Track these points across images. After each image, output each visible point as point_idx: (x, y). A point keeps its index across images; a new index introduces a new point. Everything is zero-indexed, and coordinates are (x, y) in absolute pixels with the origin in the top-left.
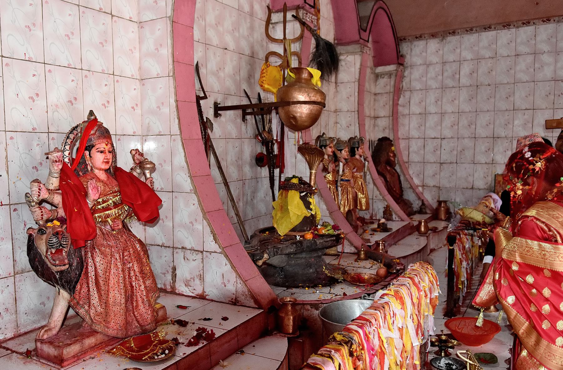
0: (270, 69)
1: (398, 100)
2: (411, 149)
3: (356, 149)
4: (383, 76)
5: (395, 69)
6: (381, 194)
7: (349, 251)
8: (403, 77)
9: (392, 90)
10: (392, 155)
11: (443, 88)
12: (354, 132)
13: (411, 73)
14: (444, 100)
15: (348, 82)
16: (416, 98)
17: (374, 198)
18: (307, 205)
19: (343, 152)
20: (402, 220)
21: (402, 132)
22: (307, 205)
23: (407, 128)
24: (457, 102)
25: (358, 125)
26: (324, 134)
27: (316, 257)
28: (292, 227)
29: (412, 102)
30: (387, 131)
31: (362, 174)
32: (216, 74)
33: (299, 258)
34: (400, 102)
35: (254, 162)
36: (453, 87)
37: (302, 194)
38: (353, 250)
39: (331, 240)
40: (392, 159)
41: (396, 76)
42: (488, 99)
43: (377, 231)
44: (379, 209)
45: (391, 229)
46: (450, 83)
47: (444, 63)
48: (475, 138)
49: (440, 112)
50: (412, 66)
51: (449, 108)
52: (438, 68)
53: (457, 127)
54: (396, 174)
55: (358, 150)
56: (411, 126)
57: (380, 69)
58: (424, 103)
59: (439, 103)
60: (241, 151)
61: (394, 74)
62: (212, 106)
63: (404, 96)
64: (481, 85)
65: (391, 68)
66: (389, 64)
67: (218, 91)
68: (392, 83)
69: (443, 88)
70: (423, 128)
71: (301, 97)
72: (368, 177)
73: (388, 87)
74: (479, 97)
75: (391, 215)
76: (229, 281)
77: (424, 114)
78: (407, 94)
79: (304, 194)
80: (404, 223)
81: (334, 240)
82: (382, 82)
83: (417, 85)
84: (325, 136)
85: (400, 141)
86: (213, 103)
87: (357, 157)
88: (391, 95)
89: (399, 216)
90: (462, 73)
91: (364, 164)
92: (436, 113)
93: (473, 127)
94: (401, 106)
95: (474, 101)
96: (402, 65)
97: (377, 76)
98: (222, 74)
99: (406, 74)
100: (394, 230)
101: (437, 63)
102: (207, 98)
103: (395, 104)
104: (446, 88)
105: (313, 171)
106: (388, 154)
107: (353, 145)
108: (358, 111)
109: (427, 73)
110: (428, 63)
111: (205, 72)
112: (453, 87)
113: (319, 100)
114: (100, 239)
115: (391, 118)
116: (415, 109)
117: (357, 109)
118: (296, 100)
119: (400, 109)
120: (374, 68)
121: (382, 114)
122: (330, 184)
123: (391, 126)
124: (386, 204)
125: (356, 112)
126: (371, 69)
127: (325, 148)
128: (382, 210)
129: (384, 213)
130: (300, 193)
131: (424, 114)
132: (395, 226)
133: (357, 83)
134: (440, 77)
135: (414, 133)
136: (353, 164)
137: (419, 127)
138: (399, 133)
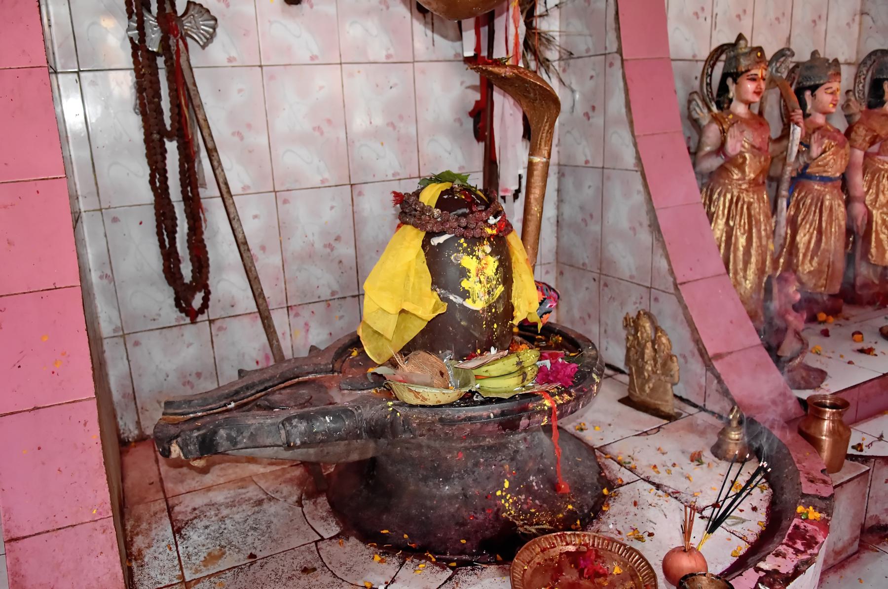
19: (820, 93)
26: (740, 37)
84: (742, 42)
127: (735, 81)
130: (430, 235)
136: (870, 130)
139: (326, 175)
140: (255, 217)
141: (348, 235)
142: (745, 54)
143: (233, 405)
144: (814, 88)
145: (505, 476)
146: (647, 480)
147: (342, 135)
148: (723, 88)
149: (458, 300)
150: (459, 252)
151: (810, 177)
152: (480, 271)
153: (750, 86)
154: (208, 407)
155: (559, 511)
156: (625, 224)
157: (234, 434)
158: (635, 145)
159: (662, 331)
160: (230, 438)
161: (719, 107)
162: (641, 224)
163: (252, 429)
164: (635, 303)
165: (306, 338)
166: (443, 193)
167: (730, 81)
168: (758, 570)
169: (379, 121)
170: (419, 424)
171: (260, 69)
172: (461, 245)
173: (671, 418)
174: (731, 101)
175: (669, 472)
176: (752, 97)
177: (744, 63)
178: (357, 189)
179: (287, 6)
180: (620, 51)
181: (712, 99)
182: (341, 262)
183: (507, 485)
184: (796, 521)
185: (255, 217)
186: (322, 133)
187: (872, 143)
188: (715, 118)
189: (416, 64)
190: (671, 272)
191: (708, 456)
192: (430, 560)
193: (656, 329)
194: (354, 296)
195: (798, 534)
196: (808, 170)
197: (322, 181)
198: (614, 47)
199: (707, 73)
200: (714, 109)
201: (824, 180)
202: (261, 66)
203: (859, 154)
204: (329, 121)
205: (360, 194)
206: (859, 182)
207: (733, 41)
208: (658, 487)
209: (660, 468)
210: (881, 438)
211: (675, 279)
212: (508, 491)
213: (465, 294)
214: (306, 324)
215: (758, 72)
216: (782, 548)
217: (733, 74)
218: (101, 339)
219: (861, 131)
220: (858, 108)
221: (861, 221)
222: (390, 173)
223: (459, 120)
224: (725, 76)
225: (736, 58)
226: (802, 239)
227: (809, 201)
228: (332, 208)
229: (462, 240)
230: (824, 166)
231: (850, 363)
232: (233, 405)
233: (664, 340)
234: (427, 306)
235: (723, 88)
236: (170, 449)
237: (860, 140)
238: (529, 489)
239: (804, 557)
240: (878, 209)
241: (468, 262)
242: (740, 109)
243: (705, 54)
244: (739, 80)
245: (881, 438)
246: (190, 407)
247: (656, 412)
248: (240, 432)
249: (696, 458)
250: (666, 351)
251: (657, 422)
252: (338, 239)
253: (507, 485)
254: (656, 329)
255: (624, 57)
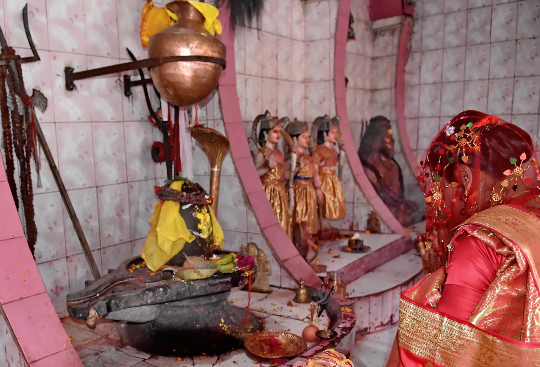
0: (152, 12)
1: (405, 65)
2: (421, 133)
3: (325, 134)
4: (383, 33)
5: (399, 21)
6: (364, 196)
7: (287, 286)
8: (411, 33)
9: (395, 51)
10: (388, 140)
11: (467, 45)
12: (329, 109)
13: (422, 27)
14: (468, 63)
15: (321, 39)
16: (428, 61)
17: (356, 201)
18: (193, 225)
19: (300, 137)
20: (393, 232)
21: (409, 109)
22: (193, 225)
23: (416, 103)
24: (486, 64)
25: (333, 100)
26: (267, 112)
27: (208, 304)
28: (167, 259)
29: (423, 67)
30: (388, 108)
31: (336, 168)
32: (69, 23)
33: (178, 307)
34: (407, 68)
35: (149, 154)
36: (482, 43)
37: (185, 207)
38: (293, 284)
39: (222, 283)
40: (389, 146)
41: (401, 31)
42: (533, 58)
43: (347, 251)
44: (361, 217)
45: (369, 248)
46: (478, 37)
47: (469, 10)
48: (512, 114)
49: (462, 79)
50: (424, 18)
51: (475, 74)
52: (461, 17)
53: (486, 100)
54: (396, 167)
55: (327, 135)
56: (422, 99)
57: (380, 24)
58: (439, 69)
59: (462, 66)
60: (125, 140)
61: (398, 30)
62: (62, 73)
63: (413, 60)
64: (522, 38)
65: (393, 21)
66: (391, 16)
67: (73, 50)
68: (396, 41)
69: (467, 45)
70: (437, 103)
71: (185, 51)
72: (346, 172)
73: (390, 48)
74: (519, 57)
75: (378, 225)
76: (12, 359)
77: (440, 84)
78: (417, 57)
79: (187, 206)
80: (397, 237)
81: (228, 283)
82: (382, 40)
83: (431, 43)
84: (268, 115)
85: (407, 121)
86: (62, 68)
87: (327, 144)
88: (394, 59)
89: (388, 227)
90: (494, 23)
91: (339, 156)
92: (456, 81)
93: (509, 99)
94: (408, 73)
95: (512, 62)
96: (410, 16)
97: (376, 34)
98: (79, 24)
99: (416, 28)
100: (374, 248)
101: (459, 10)
102: (39, 59)
103: (400, 71)
104: (472, 45)
105: (216, 169)
106: (383, 139)
107: (322, 127)
108: (334, 80)
109: (445, 25)
110: (446, 11)
111: (116, 32)
112: (482, 43)
113: (216, 55)
114: (428, 170)
115: (393, 90)
116: (428, 77)
117: (332, 77)
118: (167, 55)
119: (407, 77)
120: (370, 22)
121: (382, 84)
122: (275, 185)
123: (393, 102)
124: (372, 209)
125: (332, 82)
126: (366, 23)
127: (267, 133)
128: (365, 219)
129: (369, 222)
130: (182, 204)
131: (440, 84)
132: (374, 243)
133: (333, 41)
134: (464, 31)
135: (426, 110)
136: (320, 155)
137: (433, 101)
138: (406, 111)
139: (85, 182)
140: (52, 205)
141: (95, 215)
142: (271, 120)
143: (98, 295)
144: (297, 136)
145: (221, 317)
146: (274, 315)
147: (92, 160)
148: (262, 136)
149: (197, 234)
150: (195, 211)
151: (300, 178)
152: (205, 220)
153: (274, 135)
154: (89, 296)
155: (248, 329)
156: (230, 203)
157: (117, 302)
158: (234, 163)
159: (261, 251)
160: (116, 304)
161: (261, 145)
162: (240, 202)
163: (126, 299)
164: (239, 242)
165: (76, 275)
166: (183, 185)
167: (265, 133)
168: (339, 328)
169: (109, 152)
170: (199, 288)
171: (54, 124)
172: (196, 208)
173: (269, 292)
174: (265, 142)
175: (281, 311)
176: (275, 140)
177: (271, 124)
178: (100, 188)
179: (67, 91)
180: (222, 118)
181: (257, 142)
182: (92, 230)
183: (223, 321)
184: (343, 313)
185: (52, 205)
186: (83, 159)
187: (321, 161)
188: (260, 150)
189: (125, 123)
190: (259, 224)
191: (293, 303)
192: (204, 355)
193: (259, 250)
194: (98, 249)
195: (346, 317)
196: (298, 175)
197: (84, 185)
198: (219, 116)
199: (254, 129)
200: (259, 146)
201: (306, 179)
202: (55, 123)
203: (316, 166)
204: (86, 153)
205: (101, 192)
206: (318, 179)
207: (264, 113)
208: (280, 316)
209: (277, 310)
210: (354, 291)
211: (261, 227)
212: (224, 323)
213: (200, 231)
214: (76, 267)
215: (277, 128)
216: (343, 321)
217: (266, 129)
218: (90, 251)
219: (316, 155)
220: (314, 145)
221: (321, 198)
222: (114, 180)
223: (144, 152)
224: (262, 131)
225: (268, 121)
226: (299, 209)
227: (300, 190)
228: (88, 200)
229: (196, 206)
230: (306, 172)
231: (333, 261)
232: (98, 295)
233: (262, 255)
234: (187, 237)
235: (262, 136)
236: (89, 313)
237: (316, 160)
238: (231, 322)
239: (352, 322)
240: (327, 192)
241: (200, 216)
242: (270, 146)
243: (253, 119)
244: (270, 132)
245: (354, 291)
246: (81, 296)
247: (261, 291)
248: (120, 301)
249: (289, 304)
250: (264, 260)
251: (264, 295)
252: (91, 217)
253: (223, 321)
254: (259, 250)
255: (225, 121)
